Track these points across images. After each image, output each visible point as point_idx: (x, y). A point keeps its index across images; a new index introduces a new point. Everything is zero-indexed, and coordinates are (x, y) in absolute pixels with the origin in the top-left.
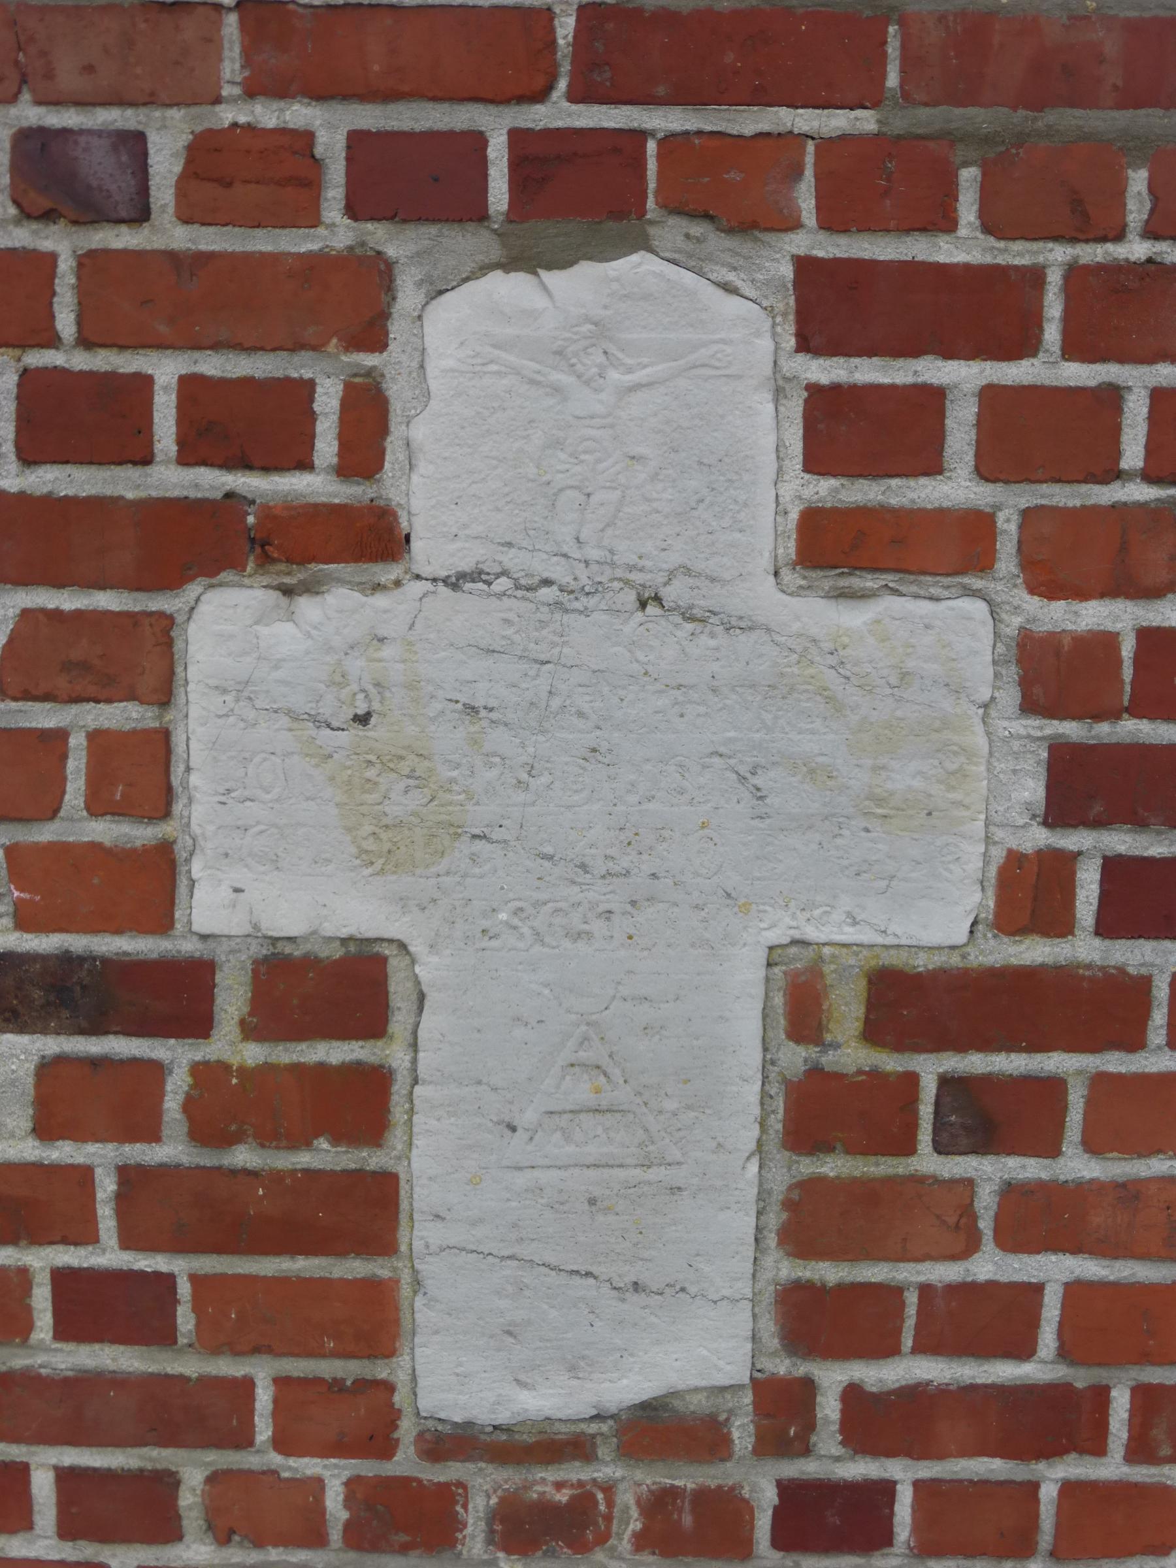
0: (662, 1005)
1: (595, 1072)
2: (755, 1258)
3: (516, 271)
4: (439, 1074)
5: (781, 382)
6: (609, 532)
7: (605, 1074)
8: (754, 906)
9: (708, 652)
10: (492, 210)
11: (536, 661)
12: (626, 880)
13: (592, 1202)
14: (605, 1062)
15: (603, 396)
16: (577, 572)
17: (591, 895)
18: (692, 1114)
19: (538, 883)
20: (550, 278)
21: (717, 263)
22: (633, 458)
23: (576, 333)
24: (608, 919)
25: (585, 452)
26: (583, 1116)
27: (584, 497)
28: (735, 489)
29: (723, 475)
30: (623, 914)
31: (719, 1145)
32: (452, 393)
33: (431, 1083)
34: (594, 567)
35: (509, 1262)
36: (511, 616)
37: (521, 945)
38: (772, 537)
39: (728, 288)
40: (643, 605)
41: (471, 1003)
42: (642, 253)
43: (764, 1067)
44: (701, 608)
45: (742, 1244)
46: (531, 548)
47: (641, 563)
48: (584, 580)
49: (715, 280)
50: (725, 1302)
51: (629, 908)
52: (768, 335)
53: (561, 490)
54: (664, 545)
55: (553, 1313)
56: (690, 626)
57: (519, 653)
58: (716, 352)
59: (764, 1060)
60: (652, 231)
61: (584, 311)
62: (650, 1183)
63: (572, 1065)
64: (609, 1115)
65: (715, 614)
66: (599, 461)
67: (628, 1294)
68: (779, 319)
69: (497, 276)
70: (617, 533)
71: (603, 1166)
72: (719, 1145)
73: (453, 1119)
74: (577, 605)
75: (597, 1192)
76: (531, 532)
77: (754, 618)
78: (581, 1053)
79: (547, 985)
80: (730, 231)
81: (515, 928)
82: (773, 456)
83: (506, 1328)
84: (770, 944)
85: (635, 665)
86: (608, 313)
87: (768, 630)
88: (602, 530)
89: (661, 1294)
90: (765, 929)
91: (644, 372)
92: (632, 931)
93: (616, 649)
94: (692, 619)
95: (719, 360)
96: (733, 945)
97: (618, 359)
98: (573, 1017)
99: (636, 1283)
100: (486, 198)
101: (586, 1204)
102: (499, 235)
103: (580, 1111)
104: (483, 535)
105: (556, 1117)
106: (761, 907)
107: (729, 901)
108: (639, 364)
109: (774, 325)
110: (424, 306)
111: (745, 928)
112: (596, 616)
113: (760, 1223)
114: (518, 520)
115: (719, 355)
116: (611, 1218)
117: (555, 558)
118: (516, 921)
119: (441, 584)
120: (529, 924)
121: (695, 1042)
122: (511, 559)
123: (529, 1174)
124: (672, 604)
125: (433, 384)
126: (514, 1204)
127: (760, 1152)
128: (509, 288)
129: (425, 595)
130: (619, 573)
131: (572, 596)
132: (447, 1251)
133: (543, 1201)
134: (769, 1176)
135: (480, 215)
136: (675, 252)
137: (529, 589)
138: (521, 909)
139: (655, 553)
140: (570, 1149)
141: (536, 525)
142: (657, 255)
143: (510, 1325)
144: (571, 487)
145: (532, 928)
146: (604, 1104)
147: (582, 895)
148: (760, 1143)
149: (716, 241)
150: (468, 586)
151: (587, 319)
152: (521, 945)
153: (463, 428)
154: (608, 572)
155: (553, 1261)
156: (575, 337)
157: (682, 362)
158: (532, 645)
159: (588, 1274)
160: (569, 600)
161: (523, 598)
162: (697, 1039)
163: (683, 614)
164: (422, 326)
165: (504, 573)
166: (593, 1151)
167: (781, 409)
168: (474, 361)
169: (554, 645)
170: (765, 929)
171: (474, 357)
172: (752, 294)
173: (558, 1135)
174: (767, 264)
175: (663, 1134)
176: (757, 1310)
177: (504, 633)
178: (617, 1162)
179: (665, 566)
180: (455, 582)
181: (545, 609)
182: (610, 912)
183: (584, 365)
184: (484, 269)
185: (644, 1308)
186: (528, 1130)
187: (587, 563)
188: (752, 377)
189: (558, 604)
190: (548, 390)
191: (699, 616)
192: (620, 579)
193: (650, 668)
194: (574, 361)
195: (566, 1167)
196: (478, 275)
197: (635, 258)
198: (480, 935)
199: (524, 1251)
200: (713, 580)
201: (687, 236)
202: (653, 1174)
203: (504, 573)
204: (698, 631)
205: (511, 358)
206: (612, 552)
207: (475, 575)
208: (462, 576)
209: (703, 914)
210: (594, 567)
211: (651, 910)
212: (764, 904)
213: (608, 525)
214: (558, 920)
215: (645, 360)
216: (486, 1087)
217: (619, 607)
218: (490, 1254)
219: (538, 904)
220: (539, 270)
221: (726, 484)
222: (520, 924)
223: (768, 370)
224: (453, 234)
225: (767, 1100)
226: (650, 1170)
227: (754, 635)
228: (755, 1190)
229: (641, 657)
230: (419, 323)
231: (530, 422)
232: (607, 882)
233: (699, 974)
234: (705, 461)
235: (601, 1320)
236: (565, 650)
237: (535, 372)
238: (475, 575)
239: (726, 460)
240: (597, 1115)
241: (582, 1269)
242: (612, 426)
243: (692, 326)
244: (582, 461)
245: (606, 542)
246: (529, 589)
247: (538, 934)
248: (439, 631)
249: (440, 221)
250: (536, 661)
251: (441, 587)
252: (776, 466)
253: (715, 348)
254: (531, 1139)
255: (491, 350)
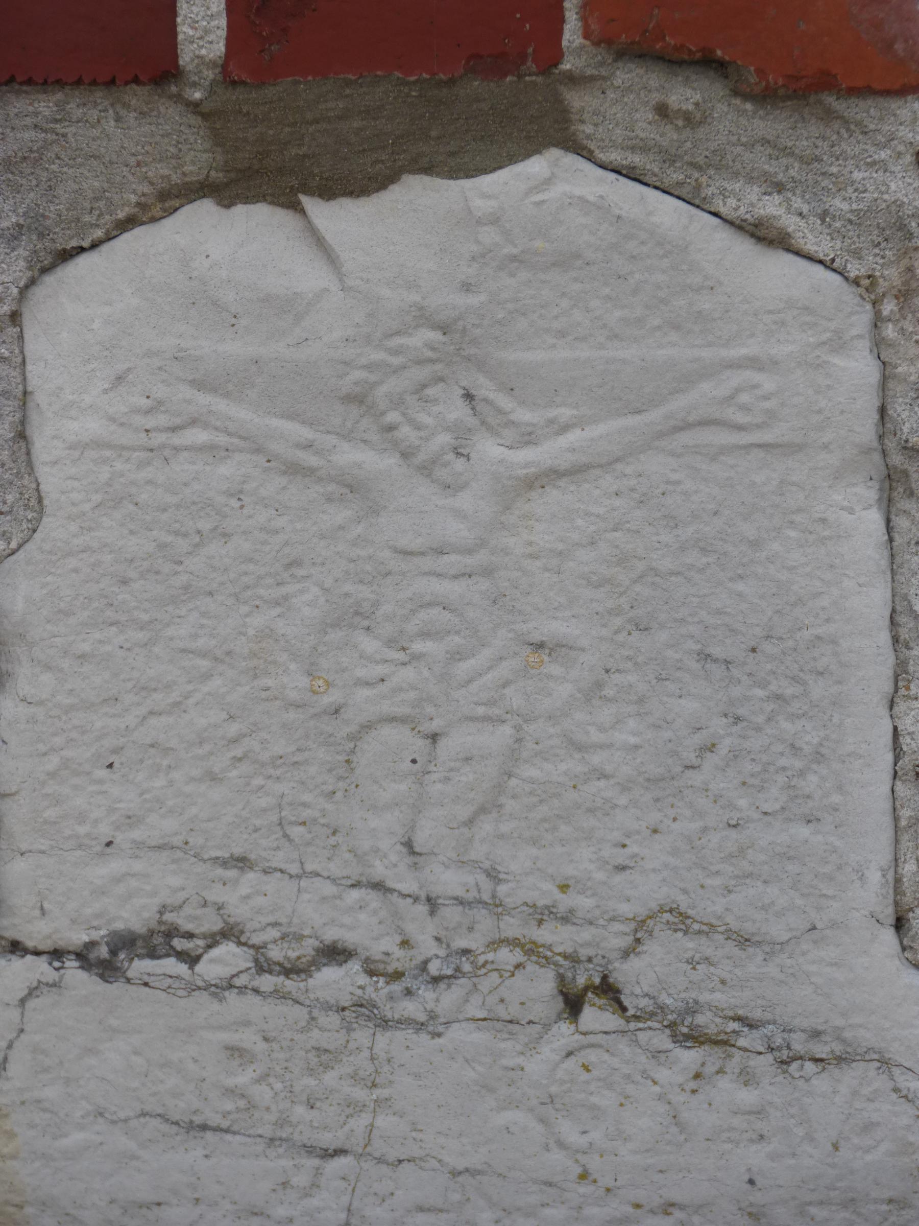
3: (247, 200)
5: (897, 459)
6: (486, 826)
9: (737, 1121)
10: (186, 57)
11: (309, 1150)
15: (464, 501)
16: (411, 928)
20: (333, 217)
21: (736, 174)
22: (540, 646)
23: (396, 352)
25: (425, 635)
27: (421, 744)
28: (793, 717)
29: (763, 685)
32: (97, 498)
34: (451, 914)
36: (248, 1038)
38: (886, 836)
39: (766, 236)
40: (573, 1005)
42: (555, 153)
44: (716, 1010)
46: (294, 869)
47: (565, 902)
48: (427, 947)
49: (732, 215)
52: (864, 345)
53: (368, 727)
54: (621, 857)
56: (690, 1057)
57: (267, 1130)
58: (738, 390)
60: (575, 99)
61: (415, 297)
65: (751, 1025)
66: (457, 656)
68: (889, 307)
69: (204, 210)
70: (505, 828)
74: (410, 1008)
76: (296, 832)
77: (847, 1034)
80: (765, 97)
82: (884, 637)
85: (557, 1157)
86: (474, 300)
87: (885, 1063)
88: (470, 822)
91: (563, 441)
93: (509, 1116)
94: (695, 1038)
95: (745, 408)
97: (500, 411)
100: (174, 26)
102: (205, 116)
104: (177, 841)
108: (551, 421)
109: (878, 321)
110: (24, 291)
112: (458, 1034)
114: (264, 802)
115: (744, 398)
117: (355, 894)
119: (71, 963)
122: (246, 898)
124: (644, 1002)
125: (51, 480)
128: (232, 244)
129: (32, 992)
130: (512, 927)
131: (397, 987)
135: (152, 64)
136: (633, 149)
137: (290, 970)
139: (600, 876)
141: (306, 814)
142: (590, 157)
144: (392, 719)
149: (733, 123)
150: (140, 967)
151: (422, 317)
153: (125, 582)
154: (485, 922)
156: (396, 361)
157: (654, 415)
158: (300, 1110)
160: (391, 998)
161: (279, 995)
163: (672, 1026)
164: (21, 337)
165: (230, 933)
167: (902, 523)
168: (150, 422)
169: (354, 1107)
171: (148, 412)
172: (824, 247)
174: (858, 176)
177: (230, 1082)
179: (625, 909)
180: (106, 959)
181: (333, 1020)
183: (418, 427)
184: (170, 198)
187: (432, 903)
188: (825, 447)
189: (362, 1009)
190: (331, 487)
191: (712, 1030)
192: (514, 943)
193: (594, 1163)
194: (392, 417)
196: (156, 211)
197: (536, 166)
200: (745, 941)
201: (662, 111)
203: (230, 933)
204: (710, 1069)
205: (240, 414)
206: (493, 875)
207: (158, 940)
208: (127, 943)
210: (451, 914)
213: (483, 810)
215: (565, 413)
217: (514, 1011)
220: (305, 199)
221: (769, 707)
223: (865, 429)
224: (94, 114)
227: (850, 1076)
229: (573, 1138)
230: (13, 331)
231: (289, 565)
234: (716, 651)
236: (384, 1121)
237: (298, 446)
238: (158, 940)
239: (768, 647)
242: (488, 572)
243: (677, 327)
244: (417, 657)
245: (478, 852)
246: (290, 970)
248: (67, 1081)
249: (60, 83)
250: (309, 1150)
251: (73, 972)
252: (891, 660)
253: (736, 379)
255: (187, 392)
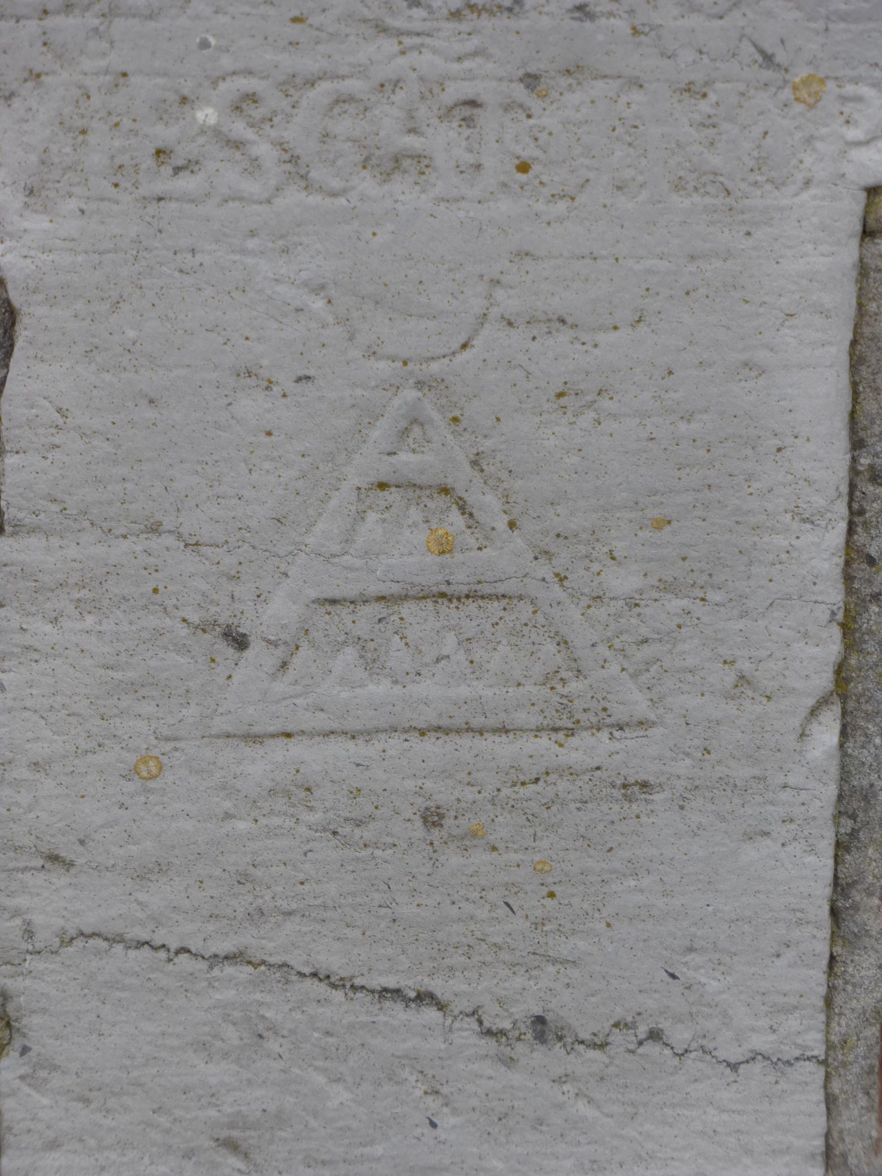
0: (602, 338)
1: (441, 501)
2: (832, 959)
4: (55, 507)
7: (463, 509)
8: (831, 85)
12: (513, 23)
13: (432, 818)
14: (462, 477)
17: (427, 61)
18: (676, 604)
19: (293, 31)
24: (468, 121)
26: (407, 609)
30: (507, 108)
31: (743, 679)
33: (33, 530)
35: (229, 970)
37: (252, 187)
41: (131, 334)
43: (852, 486)
45: (799, 923)
50: (757, 1067)
51: (519, 92)
55: (340, 1095)
59: (854, 471)
62: (572, 773)
63: (382, 486)
64: (471, 607)
67: (520, 1048)
71: (458, 731)
72: (743, 679)
73: (90, 620)
75: (444, 793)
78: (404, 457)
79: (319, 289)
81: (238, 144)
83: (225, 1133)
84: (871, 181)
89: (602, 1046)
90: (858, 144)
92: (529, 152)
96: (778, 184)
98: (383, 367)
99: (540, 1020)
101: (419, 823)
103: (405, 598)
105: (344, 612)
106: (850, 89)
107: (768, 75)
111: (810, 140)
113: (843, 871)
116: (480, 858)
118: (239, 128)
120: (273, 133)
121: (683, 427)
123: (278, 751)
126: (242, 826)
127: (844, 698)
132: (79, 943)
133: (315, 817)
134: (866, 755)
138: (253, 98)
140: (380, 688)
143: (232, 1126)
145: (281, 145)
146: (461, 580)
147: (401, 61)
148: (842, 675)
152: (252, 187)
155: (333, 961)
159: (424, 998)
162: (688, 418)
166: (433, 694)
170: (858, 144)
173: (350, 654)
175: (602, 649)
176: (836, 1086)
178: (493, 722)
182: (473, 103)
185: (560, 1080)
186: (275, 644)
195: (368, 734)
198: (149, 162)
199: (271, 942)
202: (583, 750)
209: (704, 106)
211: (574, 98)
212: (856, 81)
214: (344, 125)
216: (169, 540)
218: (185, 950)
219: (294, 84)
222: (250, 134)
225: (861, 569)
226: (574, 741)
228: (831, 791)
232: (465, 27)
233: (692, 258)
235: (455, 1112)
240: (444, 607)
241: (410, 984)
247: (294, 159)
254: (284, 665)
